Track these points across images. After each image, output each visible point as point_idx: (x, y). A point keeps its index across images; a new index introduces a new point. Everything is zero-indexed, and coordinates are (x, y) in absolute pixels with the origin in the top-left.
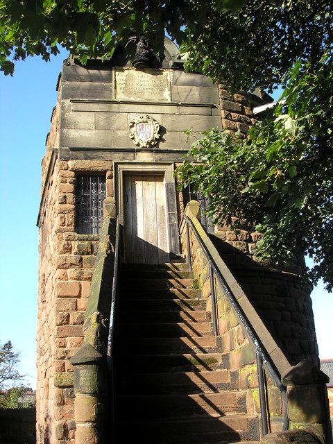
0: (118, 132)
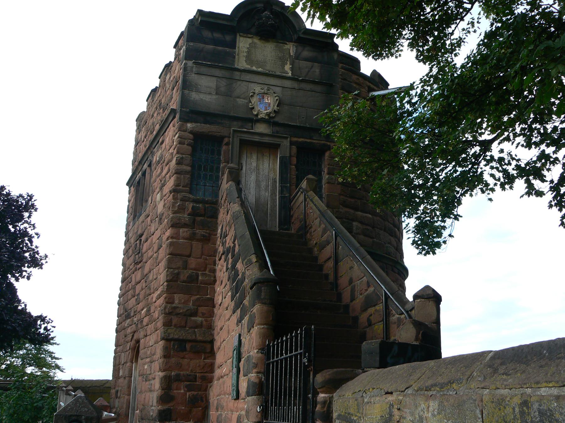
0: (238, 100)
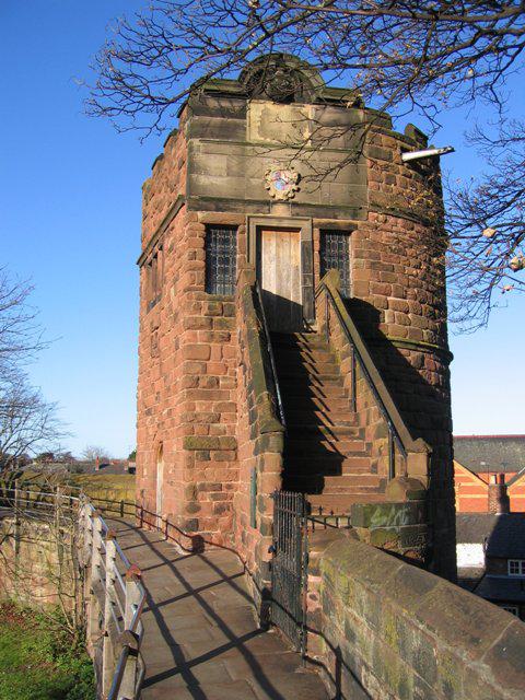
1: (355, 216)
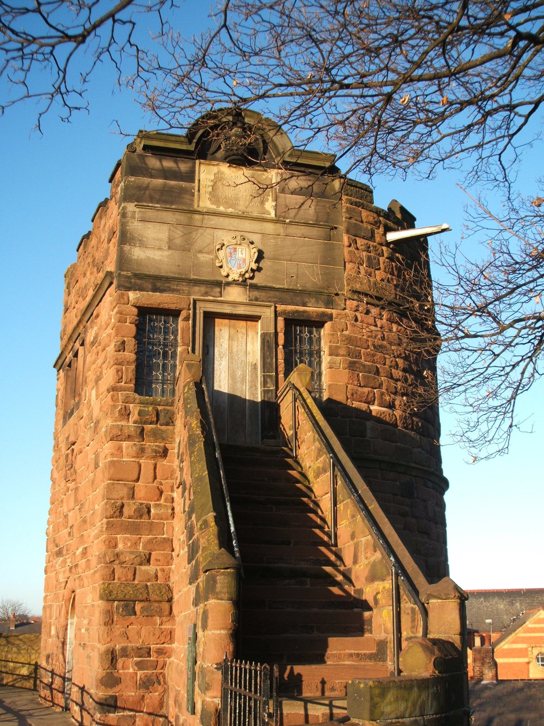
0: (199, 255)
1: (329, 303)
